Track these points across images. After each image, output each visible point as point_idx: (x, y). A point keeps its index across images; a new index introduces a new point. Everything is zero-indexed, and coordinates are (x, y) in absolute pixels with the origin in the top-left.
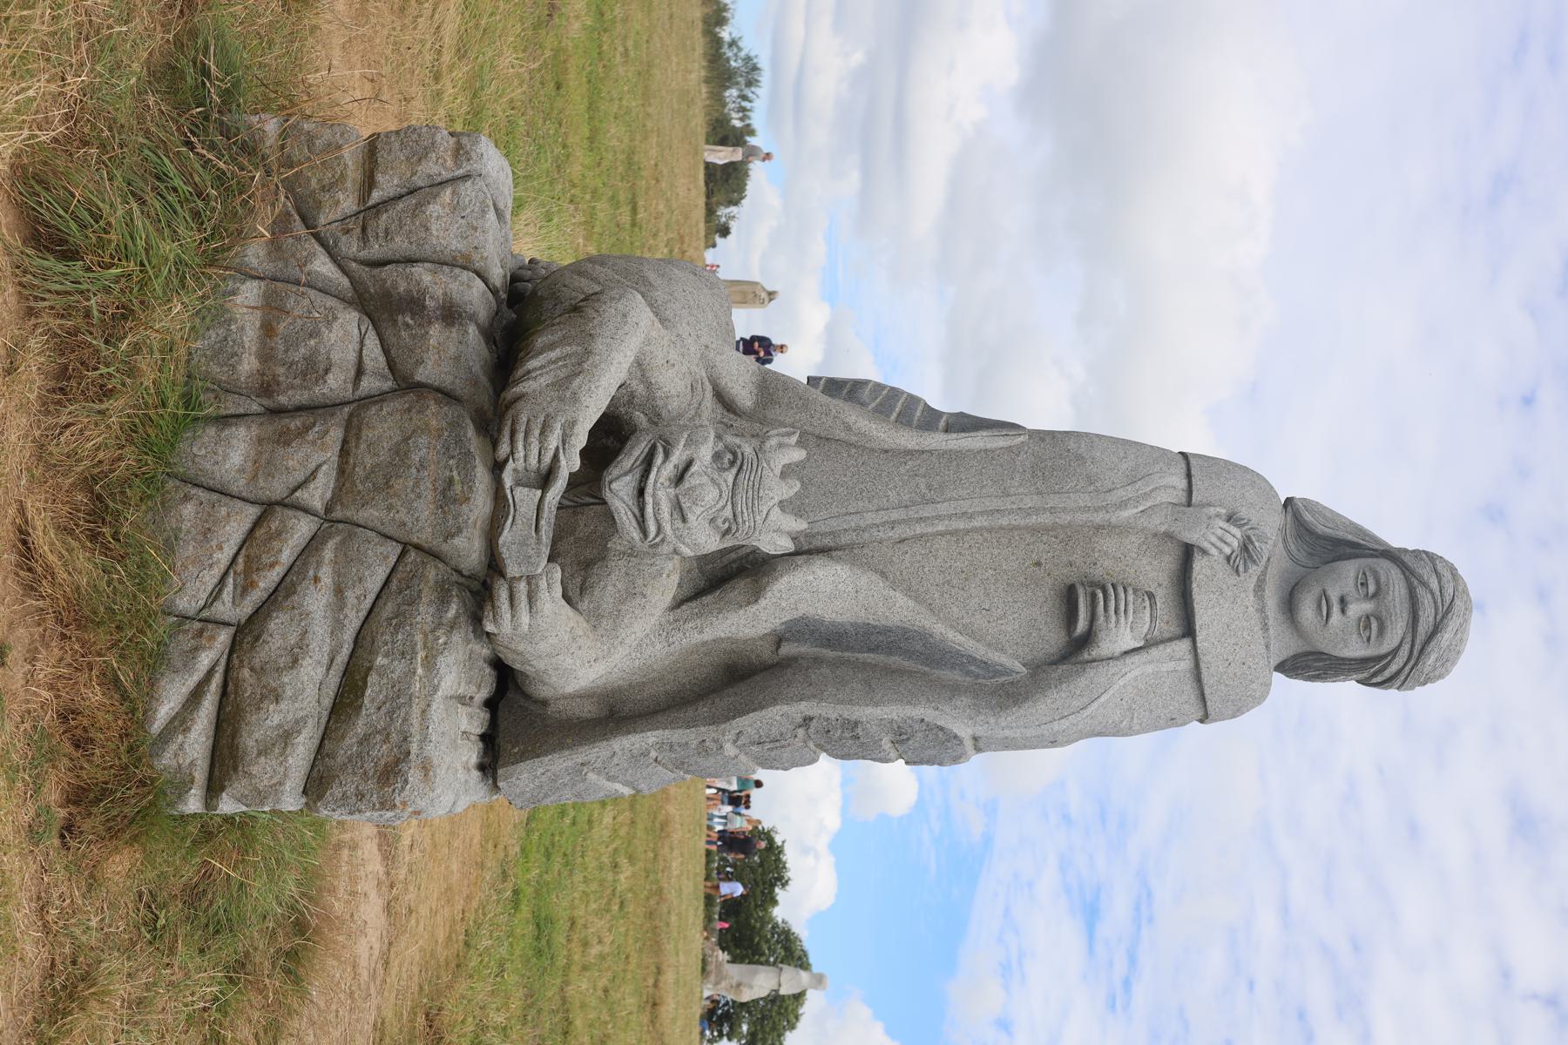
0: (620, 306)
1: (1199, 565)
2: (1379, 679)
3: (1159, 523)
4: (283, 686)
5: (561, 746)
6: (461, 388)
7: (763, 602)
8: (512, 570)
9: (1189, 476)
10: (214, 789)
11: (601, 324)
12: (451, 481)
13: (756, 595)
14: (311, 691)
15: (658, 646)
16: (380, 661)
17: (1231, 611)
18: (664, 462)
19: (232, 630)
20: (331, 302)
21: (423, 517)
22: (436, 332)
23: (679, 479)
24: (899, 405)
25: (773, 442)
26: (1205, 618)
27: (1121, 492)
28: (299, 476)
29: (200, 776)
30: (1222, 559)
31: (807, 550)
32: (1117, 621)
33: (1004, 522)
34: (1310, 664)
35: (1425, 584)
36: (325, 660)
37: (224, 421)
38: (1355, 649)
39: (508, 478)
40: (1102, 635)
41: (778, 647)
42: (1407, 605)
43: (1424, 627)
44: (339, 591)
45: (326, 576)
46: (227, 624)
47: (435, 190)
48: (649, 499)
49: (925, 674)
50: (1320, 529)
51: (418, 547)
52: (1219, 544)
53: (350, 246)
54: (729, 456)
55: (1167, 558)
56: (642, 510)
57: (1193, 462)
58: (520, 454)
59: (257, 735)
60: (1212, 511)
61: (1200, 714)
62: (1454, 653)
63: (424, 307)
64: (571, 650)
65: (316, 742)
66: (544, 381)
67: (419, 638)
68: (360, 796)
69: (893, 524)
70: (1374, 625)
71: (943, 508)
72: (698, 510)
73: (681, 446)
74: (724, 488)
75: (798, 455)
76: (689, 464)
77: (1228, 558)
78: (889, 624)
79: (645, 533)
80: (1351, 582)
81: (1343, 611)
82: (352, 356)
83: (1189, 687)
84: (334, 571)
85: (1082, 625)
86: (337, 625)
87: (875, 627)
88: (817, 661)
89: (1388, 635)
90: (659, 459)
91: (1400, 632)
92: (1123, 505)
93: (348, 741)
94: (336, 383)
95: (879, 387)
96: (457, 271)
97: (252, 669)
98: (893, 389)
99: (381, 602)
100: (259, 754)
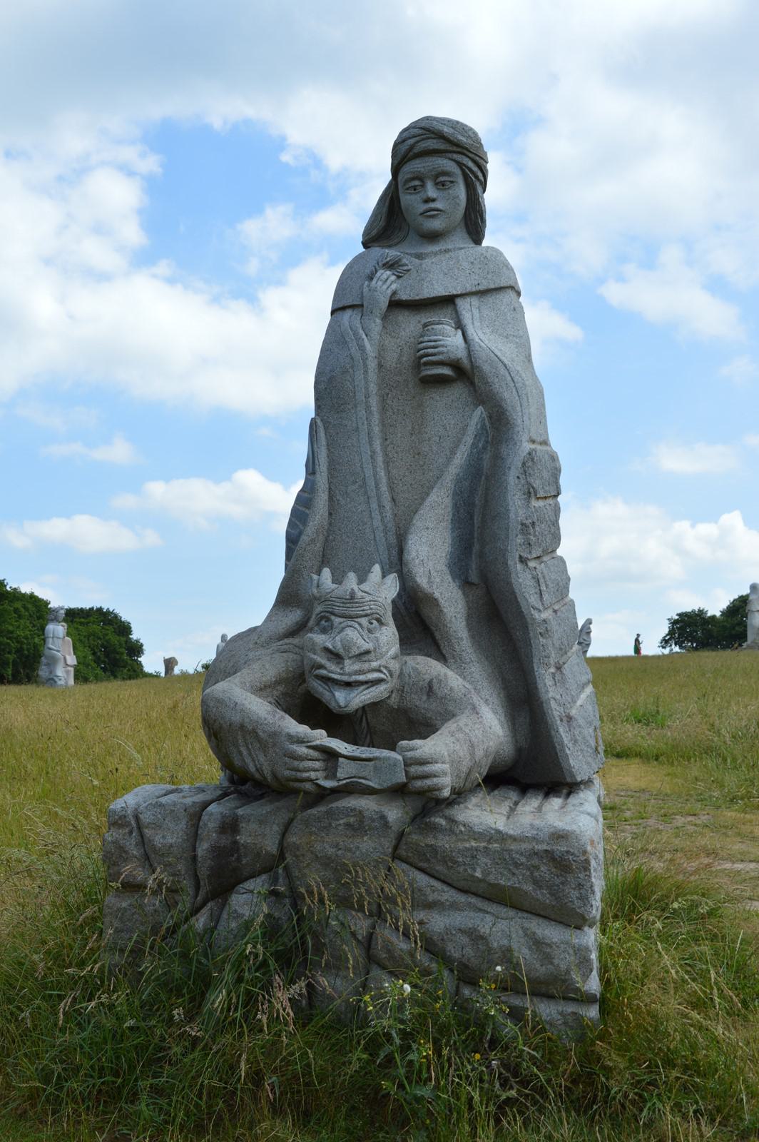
0: (211, 705)
1: (404, 296)
3: (376, 325)
4: (501, 947)
6: (283, 816)
8: (402, 778)
11: (223, 718)
12: (348, 825)
13: (434, 602)
14: (502, 925)
16: (478, 874)
17: (438, 272)
18: (325, 668)
19: (462, 983)
20: (225, 916)
21: (373, 845)
22: (242, 839)
25: (315, 591)
27: (353, 350)
29: (571, 1008)
30: (400, 281)
31: (398, 563)
32: (443, 346)
33: (376, 429)
34: (474, 223)
35: (412, 147)
36: (481, 915)
38: (461, 192)
39: (329, 784)
40: (452, 356)
42: (427, 159)
43: (440, 145)
44: (430, 906)
46: (458, 987)
47: (146, 841)
48: (354, 678)
49: (487, 478)
50: (382, 223)
51: (396, 848)
52: (388, 283)
54: (323, 622)
55: (400, 318)
57: (336, 307)
58: (313, 775)
59: (538, 966)
60: (366, 290)
61: (512, 294)
62: (455, 125)
64: (476, 729)
65: (541, 920)
66: (262, 759)
68: (580, 886)
69: (381, 507)
70: (442, 179)
71: (369, 472)
73: (315, 657)
75: (326, 572)
76: (327, 650)
77: (399, 277)
78: (450, 505)
79: (378, 682)
80: (413, 197)
81: (433, 200)
83: (490, 299)
85: (446, 371)
86: (454, 906)
87: (454, 515)
88: (481, 555)
89: (448, 169)
90: (323, 672)
91: (445, 161)
92: (362, 348)
93: (540, 896)
96: (201, 823)
100: (552, 963)
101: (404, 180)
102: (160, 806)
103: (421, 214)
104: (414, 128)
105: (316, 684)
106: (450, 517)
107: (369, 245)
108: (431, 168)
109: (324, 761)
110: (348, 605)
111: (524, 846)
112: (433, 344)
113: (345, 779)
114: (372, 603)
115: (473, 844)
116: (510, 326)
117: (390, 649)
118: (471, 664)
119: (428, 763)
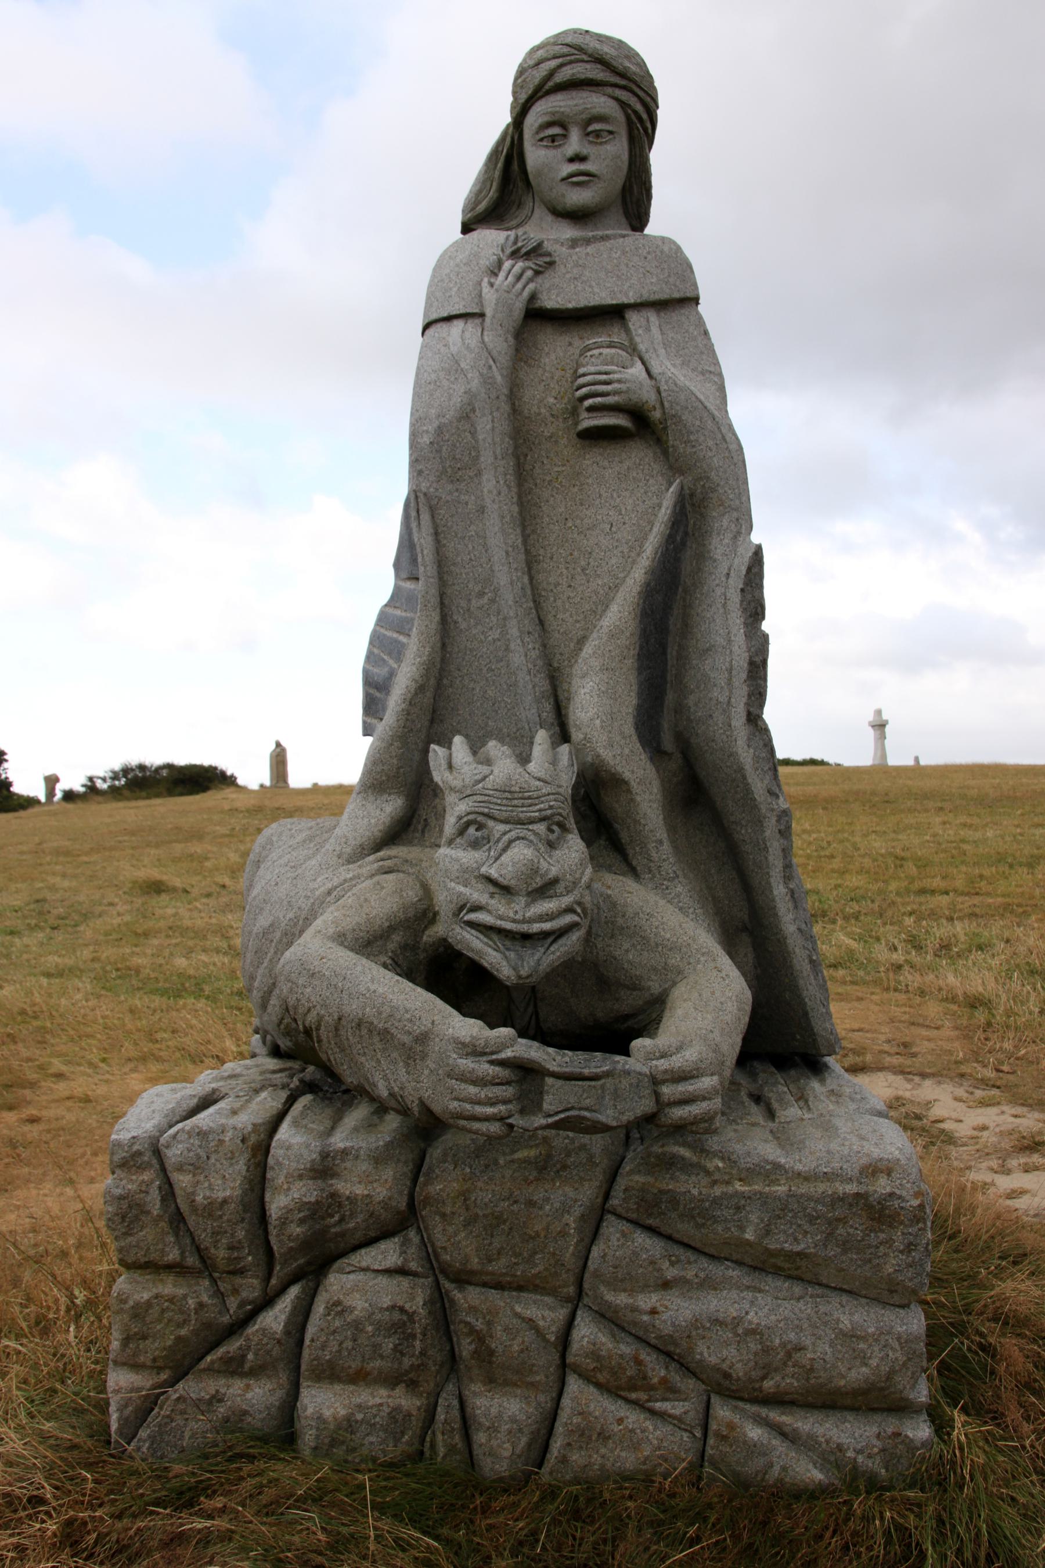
1: (551, 301)
2: (650, 131)
5: (794, 989)
7: (627, 775)
8: (646, 1105)
9: (449, 319)
10: (901, 1408)
14: (787, 1309)
15: (679, 889)
19: (715, 1399)
20: (319, 1308)
23: (504, 890)
24: (389, 634)
26: (603, 295)
28: (529, 1336)
29: (891, 1424)
32: (619, 381)
34: (633, 199)
35: (551, 74)
37: (466, 1424)
38: (618, 148)
40: (634, 398)
41: (665, 753)
42: (574, 93)
44: (666, 1285)
45: (646, 1301)
48: (536, 927)
50: (493, 193)
53: (251, 1287)
54: (471, 830)
56: (545, 935)
57: (434, 316)
63: (317, 1202)
65: (845, 1298)
67: (718, 1191)
72: (544, 865)
74: (513, 834)
82: (383, 1281)
84: (642, 1291)
86: (708, 1284)
87: (641, 648)
89: (597, 111)
91: (603, 99)
94: (416, 1297)
95: (370, 657)
97: (764, 1378)
98: (371, 643)
99: (676, 1235)
101: (536, 125)
102: (198, 1134)
103: (563, 180)
104: (555, 44)
105: (468, 936)
106: (637, 651)
107: (473, 227)
108: (580, 108)
109: (517, 1082)
110: (516, 802)
111: (821, 1187)
112: (604, 377)
113: (557, 1113)
114: (551, 797)
115: (738, 1186)
116: (704, 357)
117: (583, 873)
118: (676, 881)
119: (693, 1077)
